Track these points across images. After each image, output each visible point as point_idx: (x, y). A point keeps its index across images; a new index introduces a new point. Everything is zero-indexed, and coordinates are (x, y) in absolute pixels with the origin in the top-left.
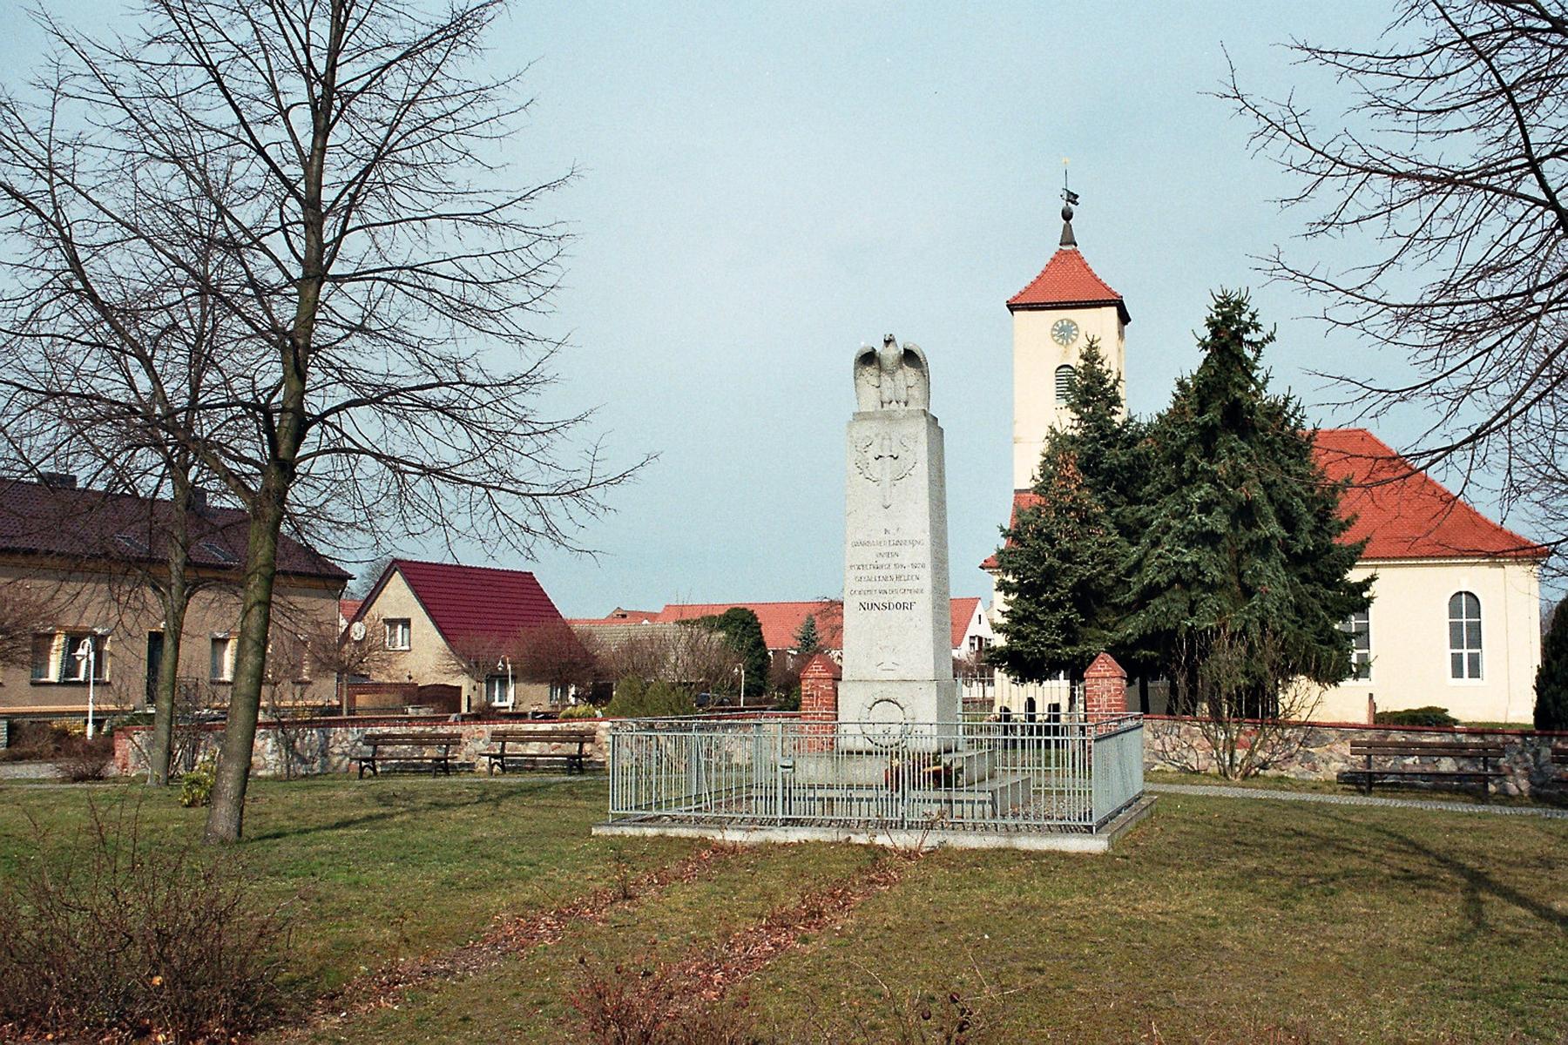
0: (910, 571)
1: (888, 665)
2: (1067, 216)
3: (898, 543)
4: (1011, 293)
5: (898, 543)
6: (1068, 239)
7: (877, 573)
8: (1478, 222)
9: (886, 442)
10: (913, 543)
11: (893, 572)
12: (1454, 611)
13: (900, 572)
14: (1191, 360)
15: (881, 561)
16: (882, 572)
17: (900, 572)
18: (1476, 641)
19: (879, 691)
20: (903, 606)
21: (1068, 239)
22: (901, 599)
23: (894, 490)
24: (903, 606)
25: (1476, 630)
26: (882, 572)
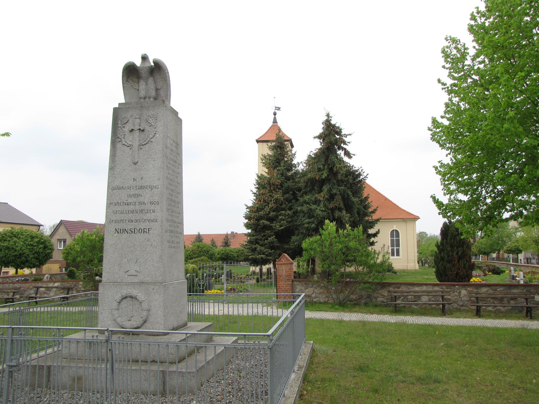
0: (148, 207)
1: (133, 272)
2: (275, 114)
3: (141, 187)
4: (257, 137)
5: (141, 187)
6: (275, 121)
7: (127, 208)
8: (154, 361)
9: (138, 121)
10: (152, 188)
11: (137, 207)
12: (392, 236)
13: (143, 207)
14: (316, 145)
15: (130, 200)
16: (131, 207)
17: (143, 207)
18: (398, 245)
19: (125, 291)
20: (144, 231)
21: (275, 121)
22: (142, 226)
23: (141, 151)
24: (144, 231)
25: (398, 241)
26: (131, 207)
